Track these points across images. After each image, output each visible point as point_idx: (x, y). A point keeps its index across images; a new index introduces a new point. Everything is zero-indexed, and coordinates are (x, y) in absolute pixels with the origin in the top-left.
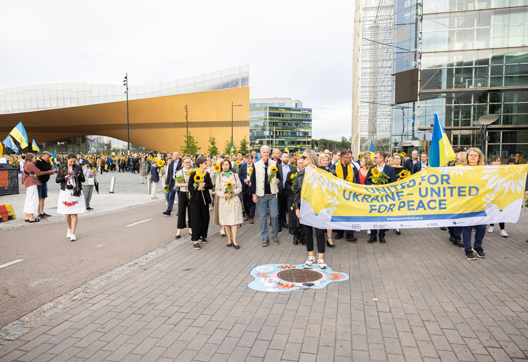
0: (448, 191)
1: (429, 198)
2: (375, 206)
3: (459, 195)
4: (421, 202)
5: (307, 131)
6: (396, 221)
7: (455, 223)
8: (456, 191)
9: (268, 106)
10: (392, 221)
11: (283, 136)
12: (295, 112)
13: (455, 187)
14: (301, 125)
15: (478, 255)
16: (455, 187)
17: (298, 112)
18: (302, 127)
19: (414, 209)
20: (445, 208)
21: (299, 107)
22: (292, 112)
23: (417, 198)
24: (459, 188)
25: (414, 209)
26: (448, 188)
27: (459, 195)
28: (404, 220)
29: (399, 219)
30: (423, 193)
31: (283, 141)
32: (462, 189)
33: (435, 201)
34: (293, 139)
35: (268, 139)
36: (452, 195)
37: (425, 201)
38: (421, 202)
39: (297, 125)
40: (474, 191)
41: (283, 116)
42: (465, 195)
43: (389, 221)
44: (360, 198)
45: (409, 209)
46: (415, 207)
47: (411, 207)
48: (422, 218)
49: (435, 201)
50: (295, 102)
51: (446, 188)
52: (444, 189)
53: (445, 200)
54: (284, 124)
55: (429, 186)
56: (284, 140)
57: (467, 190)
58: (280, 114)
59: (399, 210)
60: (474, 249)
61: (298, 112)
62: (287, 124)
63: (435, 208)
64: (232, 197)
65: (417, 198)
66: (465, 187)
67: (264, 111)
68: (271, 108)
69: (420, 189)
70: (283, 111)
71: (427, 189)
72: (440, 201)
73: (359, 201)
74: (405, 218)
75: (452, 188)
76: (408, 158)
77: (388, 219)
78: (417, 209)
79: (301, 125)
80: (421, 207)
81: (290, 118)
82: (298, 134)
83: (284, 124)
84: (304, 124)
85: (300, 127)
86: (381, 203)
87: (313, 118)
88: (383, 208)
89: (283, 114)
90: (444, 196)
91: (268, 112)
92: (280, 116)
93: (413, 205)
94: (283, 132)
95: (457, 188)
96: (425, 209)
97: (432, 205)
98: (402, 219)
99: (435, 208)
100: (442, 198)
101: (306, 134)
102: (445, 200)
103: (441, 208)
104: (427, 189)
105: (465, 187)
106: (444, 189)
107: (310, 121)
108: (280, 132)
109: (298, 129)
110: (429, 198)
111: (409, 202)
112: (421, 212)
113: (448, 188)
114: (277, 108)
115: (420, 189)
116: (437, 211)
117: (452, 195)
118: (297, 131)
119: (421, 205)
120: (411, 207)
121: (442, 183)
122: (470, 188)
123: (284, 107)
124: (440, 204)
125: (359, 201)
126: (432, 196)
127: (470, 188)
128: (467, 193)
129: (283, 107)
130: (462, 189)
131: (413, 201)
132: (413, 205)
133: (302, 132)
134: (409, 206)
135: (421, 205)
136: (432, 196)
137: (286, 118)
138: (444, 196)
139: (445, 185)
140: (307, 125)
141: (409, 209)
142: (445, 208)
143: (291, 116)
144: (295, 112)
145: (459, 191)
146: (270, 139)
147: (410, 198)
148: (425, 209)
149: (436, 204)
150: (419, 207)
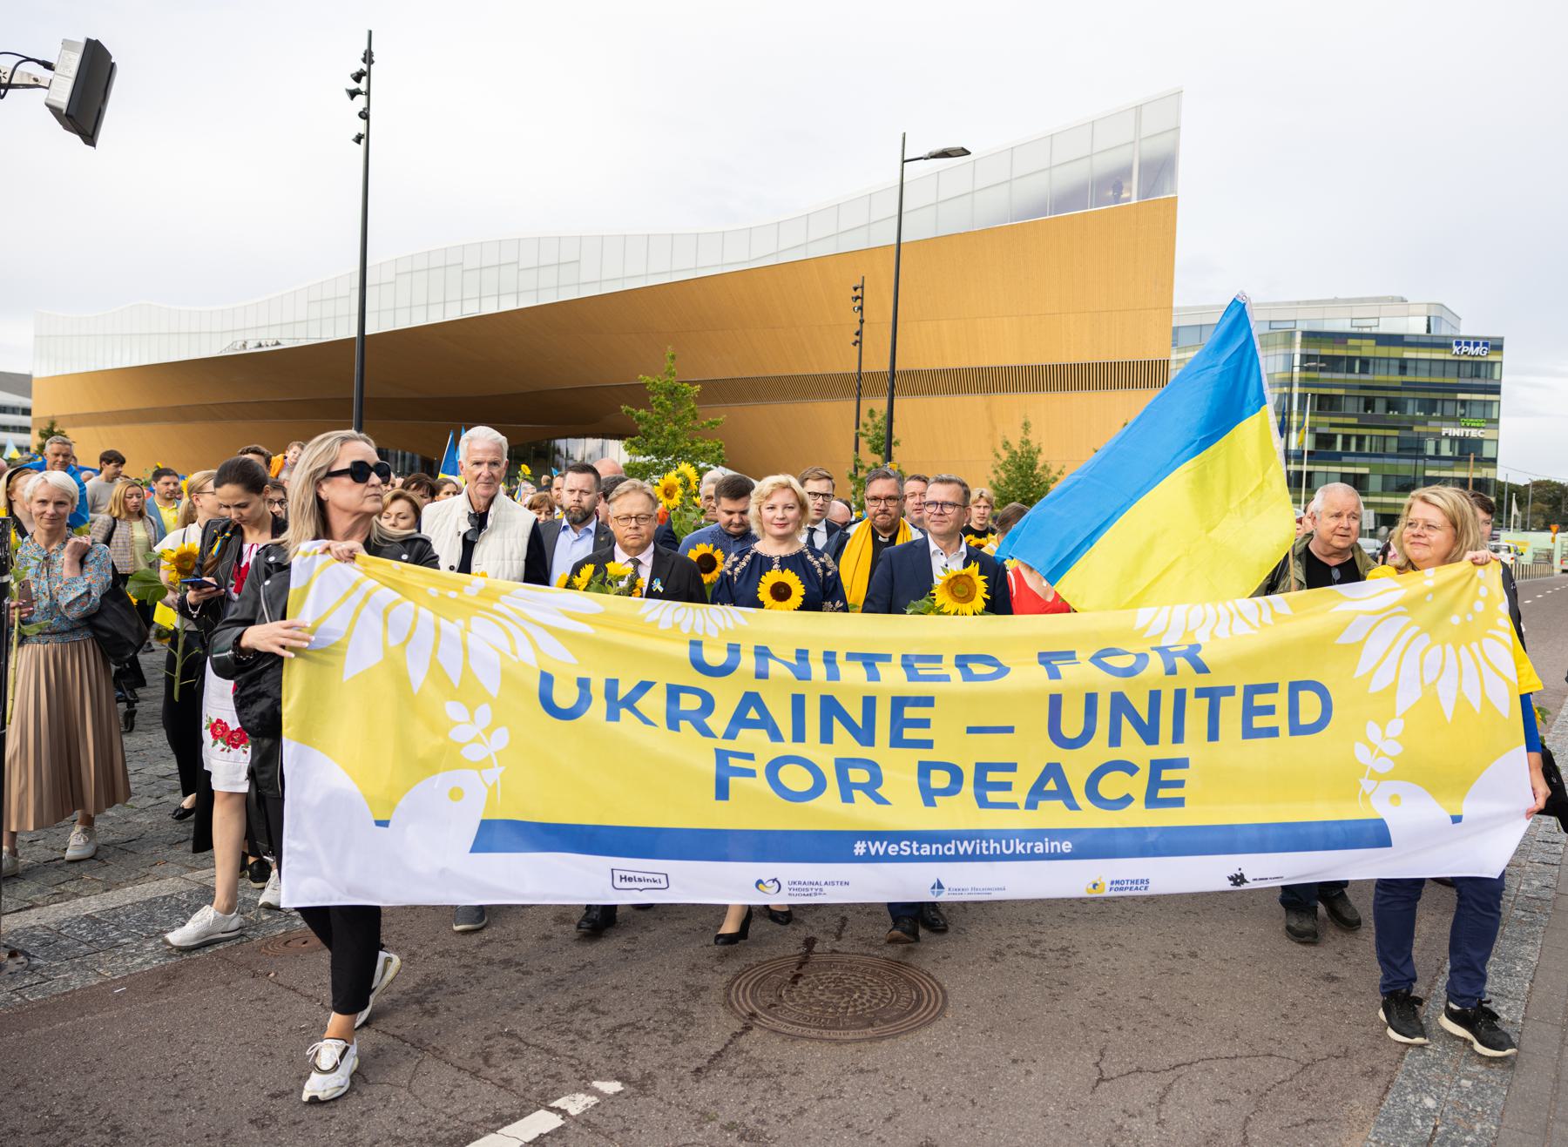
0: (1197, 711)
1: (1098, 751)
3: (1249, 732)
4: (1053, 771)
5: (1474, 433)
6: (911, 859)
7: (1238, 879)
8: (1231, 709)
9: (1304, 326)
10: (886, 858)
11: (1360, 453)
12: (1424, 354)
13: (1230, 691)
14: (1449, 407)
15: (1478, 1047)
17: (1438, 355)
18: (1455, 420)
21: (1442, 331)
22: (1409, 354)
23: (1032, 752)
24: (1251, 691)
26: (1200, 693)
27: (1249, 732)
28: (957, 858)
29: (926, 850)
30: (1072, 725)
31: (1363, 476)
33: (1131, 769)
34: (1405, 466)
35: (1298, 468)
36: (1213, 735)
37: (1077, 766)
38: (1053, 771)
39: (1429, 407)
40: (1310, 706)
41: (1364, 370)
42: (1273, 732)
43: (868, 858)
46: (1019, 795)
48: (1067, 847)
49: (1131, 769)
50: (1424, 310)
51: (1190, 695)
52: (1180, 695)
54: (1369, 404)
56: (1365, 470)
57: (1280, 700)
58: (1351, 359)
60: (1452, 1016)
61: (1438, 355)
62: (1380, 407)
63: (1127, 800)
65: (1032, 752)
66: (1272, 688)
67: (1281, 350)
68: (1311, 337)
70: (1369, 349)
71: (1091, 700)
72: (1157, 766)
75: (1213, 695)
76: (920, 536)
77: (860, 848)
78: (1032, 805)
79: (1449, 407)
80: (1051, 795)
81: (1395, 378)
82: (1430, 451)
83: (1369, 404)
84: (1463, 402)
85: (1444, 418)
86: (788, 747)
87: (1509, 381)
89: (1365, 363)
90: (1178, 737)
91: (1298, 351)
92: (1351, 370)
93: (1007, 786)
94: (1361, 439)
95: (897, 659)
96: (1073, 806)
97: (1111, 786)
98: (950, 849)
99: (1127, 800)
100: (1165, 749)
101: (1469, 450)
103: (1152, 801)
104: (1091, 700)
105: (1272, 688)
106: (1180, 695)
107: (1496, 390)
108: (1347, 438)
109: (1433, 426)
110: (1098, 751)
111: (982, 769)
112: (1052, 815)
113: (1200, 693)
114: (1340, 338)
116: (1138, 816)
117: (1213, 735)
118: (1428, 434)
119: (1051, 786)
122: (1295, 687)
123: (1374, 330)
124: (1155, 782)
126: (1115, 740)
127: (1295, 687)
128: (1280, 720)
129: (1367, 330)
131: (1012, 767)
132: (1007, 786)
133: (1453, 439)
136: (1115, 740)
137: (1378, 377)
138: (1178, 737)
140: (1477, 410)
142: (1179, 802)
143: (1364, 370)
144: (1424, 354)
145: (1249, 711)
146: (1305, 468)
147: (993, 749)
148: (1073, 806)
149: (1138, 785)
150: (1037, 794)
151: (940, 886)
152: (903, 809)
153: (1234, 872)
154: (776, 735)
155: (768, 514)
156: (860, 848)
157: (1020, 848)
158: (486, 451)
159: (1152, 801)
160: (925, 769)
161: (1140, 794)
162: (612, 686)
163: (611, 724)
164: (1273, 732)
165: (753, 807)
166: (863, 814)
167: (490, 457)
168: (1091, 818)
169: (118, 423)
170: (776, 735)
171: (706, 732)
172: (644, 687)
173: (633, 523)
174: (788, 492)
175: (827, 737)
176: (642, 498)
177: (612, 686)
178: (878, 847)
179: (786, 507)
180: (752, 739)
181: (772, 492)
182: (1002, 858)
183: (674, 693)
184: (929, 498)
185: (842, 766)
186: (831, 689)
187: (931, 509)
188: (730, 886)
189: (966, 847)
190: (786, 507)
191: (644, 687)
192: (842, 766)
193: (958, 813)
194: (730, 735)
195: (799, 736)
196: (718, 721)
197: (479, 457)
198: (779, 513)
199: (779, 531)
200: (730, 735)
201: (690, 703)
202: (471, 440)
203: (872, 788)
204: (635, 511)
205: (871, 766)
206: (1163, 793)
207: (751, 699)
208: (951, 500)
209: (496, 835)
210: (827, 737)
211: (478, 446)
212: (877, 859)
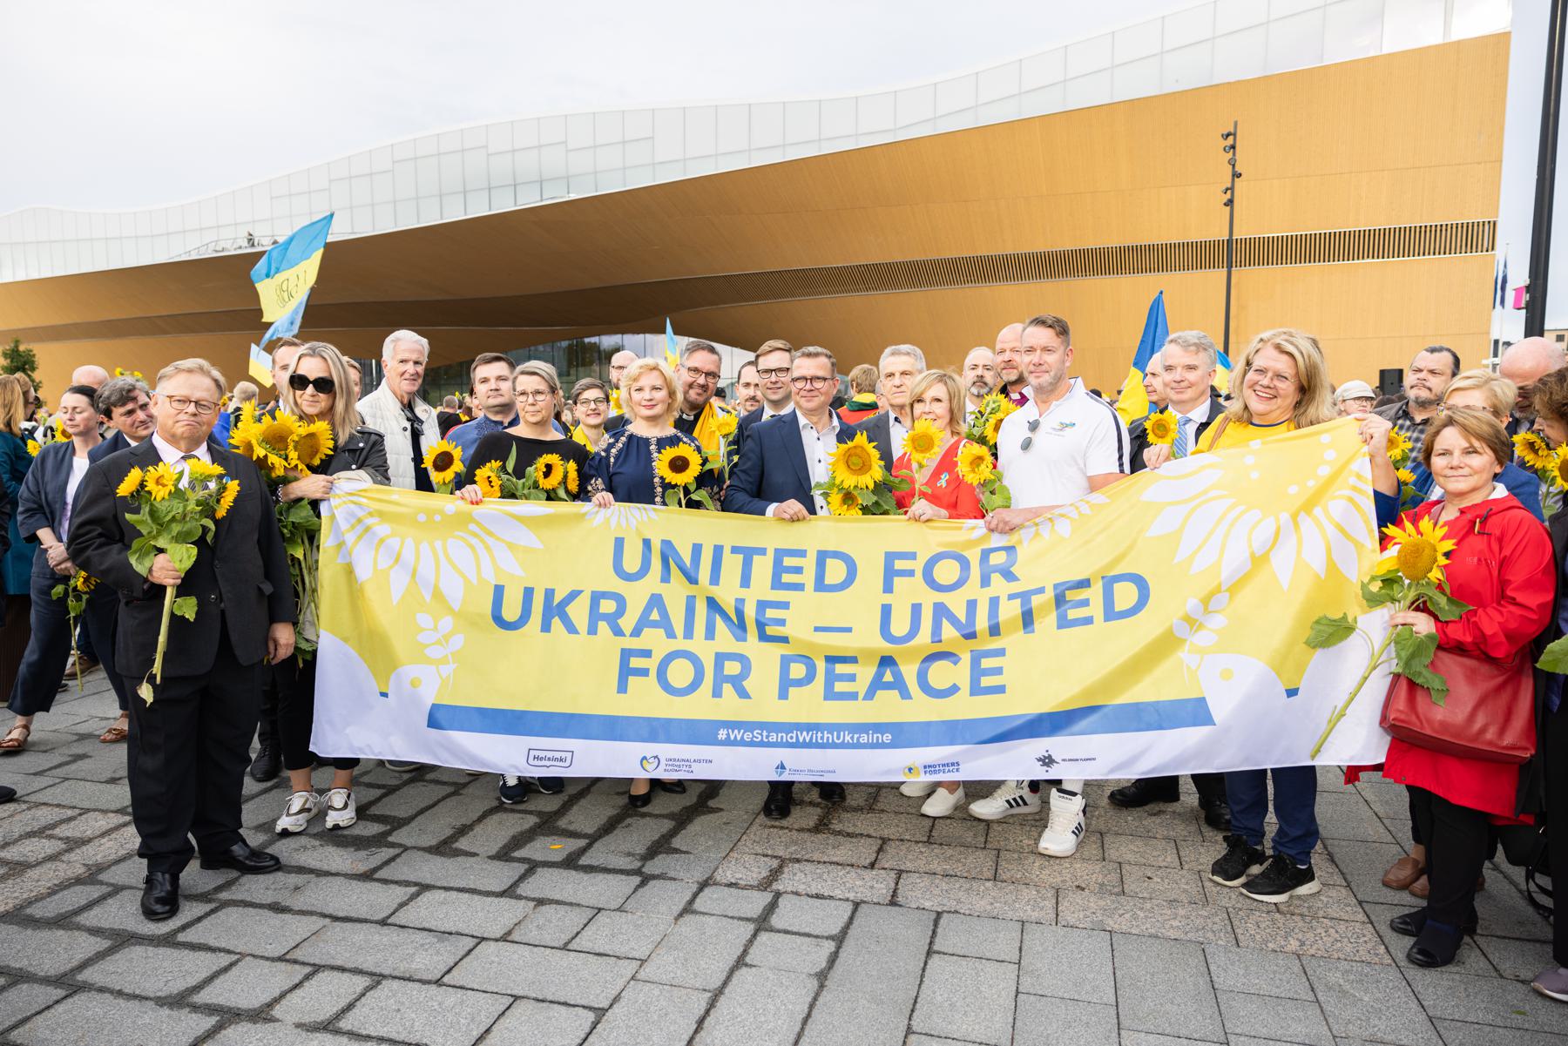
2: (647, 654)
3: (1064, 623)
13: (762, 551)
16: (762, 551)
19: (853, 696)
20: (1000, 689)
24: (780, 554)
25: (853, 696)
27: (1064, 623)
32: (788, 561)
40: (1125, 595)
42: (1088, 621)
43: (728, 742)
44: (579, 612)
45: (830, 695)
46: (861, 686)
47: (839, 687)
53: (1001, 652)
55: (929, 598)
57: (809, 564)
59: (783, 695)
63: (954, 689)
64: (872, 866)
66: (802, 553)
69: (886, 611)
71: (916, 609)
73: (571, 629)
74: (805, 736)
78: (870, 695)
86: (680, 644)
88: (680, 673)
95: (770, 554)
96: (905, 695)
97: (940, 675)
98: (792, 737)
99: (954, 689)
102: (1001, 652)
103: (976, 690)
104: (916, 609)
105: (802, 553)
115: (886, 611)
119: (655, 616)
120: (839, 687)
121: (985, 581)
122: (822, 557)
124: (977, 672)
125: (571, 629)
127: (822, 557)
130: (788, 561)
134: (831, 678)
135: (655, 616)
139: (999, 586)
141: (830, 695)
142: (1000, 689)
145: (778, 569)
148: (905, 695)
149: (960, 673)
150: (877, 685)
151: (783, 767)
152: (765, 704)
153: (1042, 753)
154: (671, 634)
155: (636, 396)
156: (722, 734)
157: (848, 738)
158: (412, 351)
159: (976, 690)
160: (786, 661)
161: (965, 685)
162: (549, 594)
163: (709, 642)
164: (1088, 621)
165: (645, 700)
166: (729, 707)
167: (414, 357)
168: (921, 709)
169: (76, 337)
170: (671, 634)
171: (618, 632)
172: (574, 595)
173: (192, 408)
174: (656, 373)
175: (710, 634)
176: (208, 382)
177: (549, 594)
178: (736, 734)
179: (654, 388)
180: (653, 639)
181: (640, 375)
182: (834, 746)
183: (597, 597)
184: (796, 374)
185: (720, 658)
186: (691, 590)
187: (800, 385)
188: (509, 757)
189: (805, 736)
190: (654, 388)
191: (574, 595)
192: (720, 658)
193: (808, 705)
194: (636, 632)
195: (689, 634)
196: (628, 622)
197: (406, 356)
198: (647, 394)
199: (534, 419)
200: (636, 632)
201: (607, 606)
202: (396, 341)
203: (737, 682)
204: (197, 395)
205: (742, 659)
206: (986, 681)
207: (656, 601)
208: (821, 373)
209: (437, 718)
210: (710, 634)
211: (402, 346)
212: (735, 743)
